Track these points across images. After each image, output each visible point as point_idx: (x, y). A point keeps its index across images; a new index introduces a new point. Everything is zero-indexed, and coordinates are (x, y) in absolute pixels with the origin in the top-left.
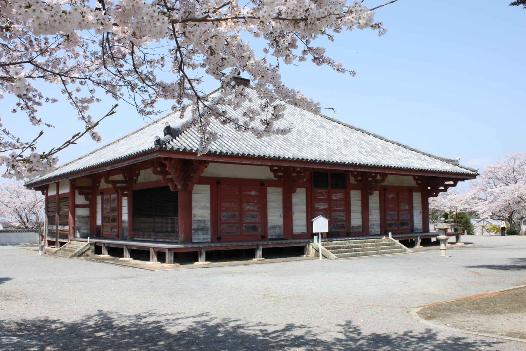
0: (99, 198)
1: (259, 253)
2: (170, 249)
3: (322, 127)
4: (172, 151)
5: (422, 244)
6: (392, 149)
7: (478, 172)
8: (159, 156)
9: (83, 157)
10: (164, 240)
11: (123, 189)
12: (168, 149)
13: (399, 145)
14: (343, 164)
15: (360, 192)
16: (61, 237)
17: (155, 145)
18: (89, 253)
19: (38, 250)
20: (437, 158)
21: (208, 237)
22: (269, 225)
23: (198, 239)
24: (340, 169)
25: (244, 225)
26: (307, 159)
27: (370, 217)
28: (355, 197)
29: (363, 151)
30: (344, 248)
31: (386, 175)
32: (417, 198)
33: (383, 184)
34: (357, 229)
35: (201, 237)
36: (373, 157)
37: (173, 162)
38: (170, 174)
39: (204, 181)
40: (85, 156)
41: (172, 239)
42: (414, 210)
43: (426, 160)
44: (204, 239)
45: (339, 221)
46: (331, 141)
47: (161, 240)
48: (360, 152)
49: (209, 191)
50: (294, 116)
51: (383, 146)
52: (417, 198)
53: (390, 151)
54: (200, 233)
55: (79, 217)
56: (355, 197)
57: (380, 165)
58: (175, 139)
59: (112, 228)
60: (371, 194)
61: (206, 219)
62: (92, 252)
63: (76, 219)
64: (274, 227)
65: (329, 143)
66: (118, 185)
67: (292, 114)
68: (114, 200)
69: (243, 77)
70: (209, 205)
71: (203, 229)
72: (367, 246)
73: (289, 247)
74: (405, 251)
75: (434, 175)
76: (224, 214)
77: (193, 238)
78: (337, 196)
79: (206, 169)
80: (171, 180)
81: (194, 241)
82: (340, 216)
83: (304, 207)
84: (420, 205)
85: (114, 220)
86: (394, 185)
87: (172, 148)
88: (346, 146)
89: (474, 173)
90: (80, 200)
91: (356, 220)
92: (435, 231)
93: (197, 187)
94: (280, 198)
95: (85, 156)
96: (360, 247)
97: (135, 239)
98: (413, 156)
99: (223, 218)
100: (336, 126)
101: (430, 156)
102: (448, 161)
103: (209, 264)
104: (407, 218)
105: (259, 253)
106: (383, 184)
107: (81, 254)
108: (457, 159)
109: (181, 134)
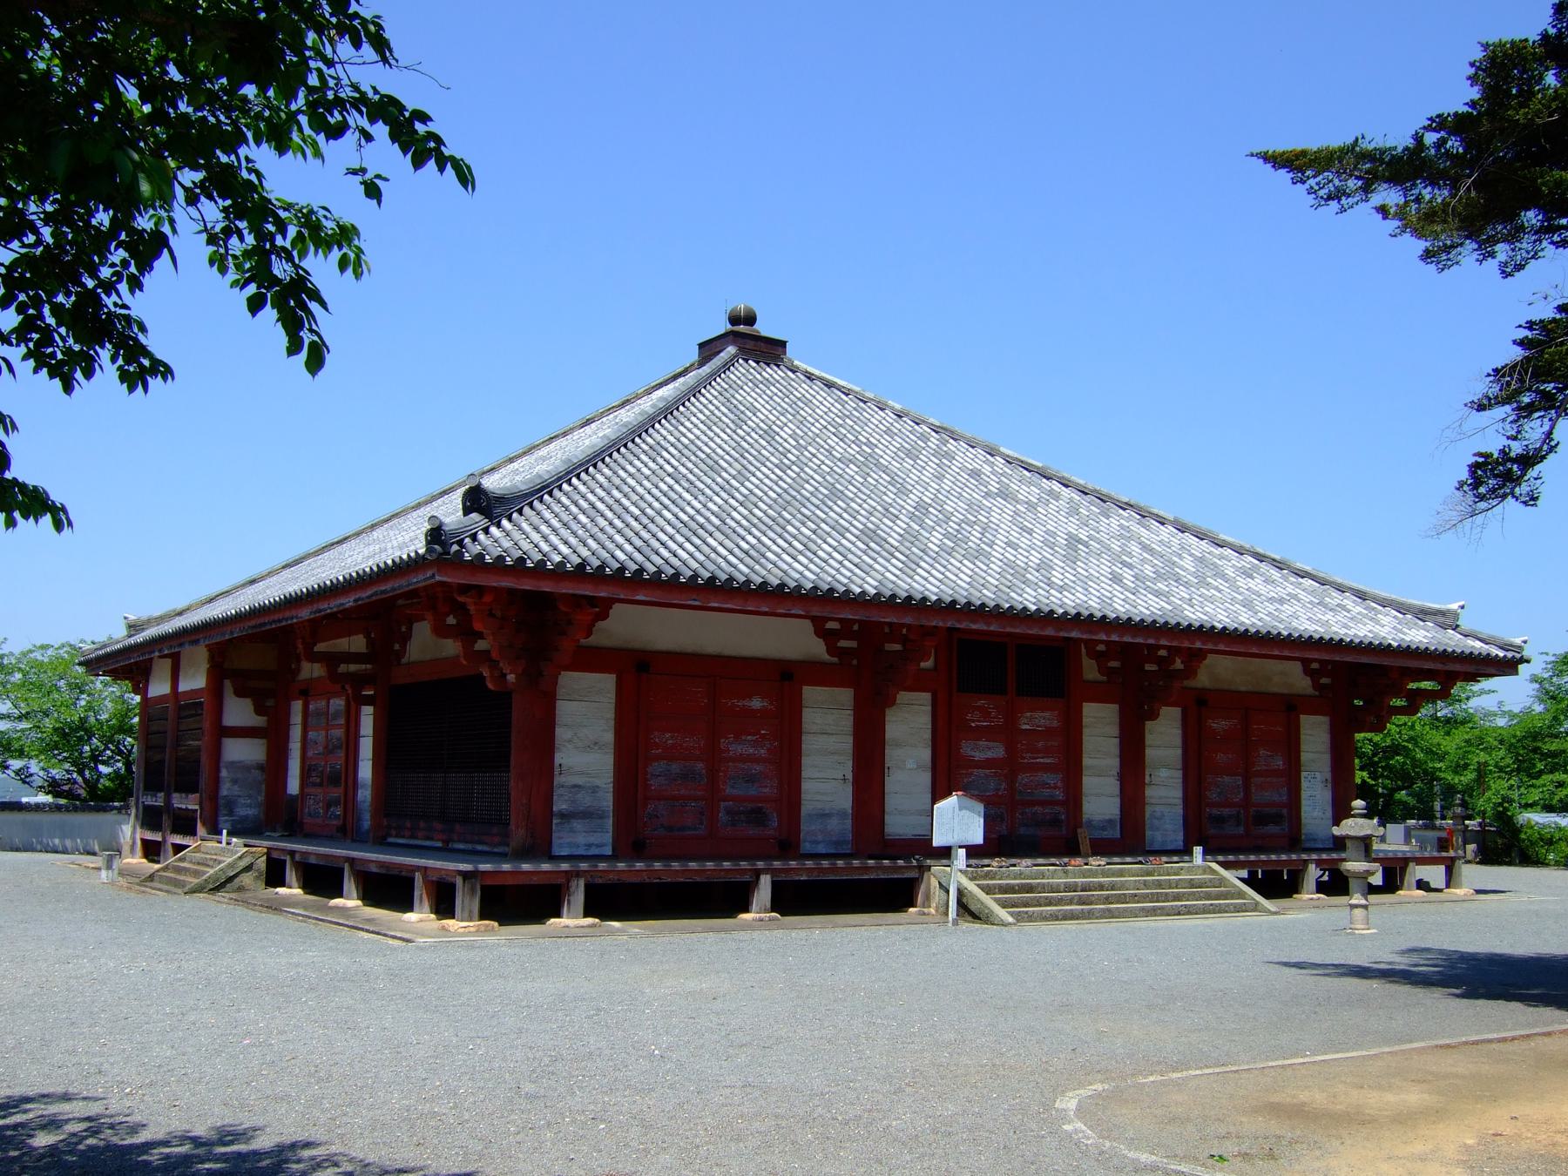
0: (297, 707)
1: (763, 892)
2: (466, 875)
3: (1005, 494)
4: (479, 562)
5: (1321, 888)
6: (1230, 572)
7: (1526, 653)
8: (438, 578)
9: (262, 578)
10: (470, 847)
11: (359, 681)
12: (467, 557)
13: (1261, 558)
14: (1046, 618)
15: (1115, 707)
16: (177, 830)
17: (428, 543)
18: (247, 879)
19: (99, 869)
20: (1385, 603)
21: (603, 839)
22: (806, 808)
23: (570, 845)
24: (1034, 631)
25: (723, 804)
26: (925, 599)
27: (1149, 792)
28: (1100, 727)
29: (1128, 575)
30: (1043, 888)
31: (1200, 655)
32: (1314, 736)
33: (1187, 683)
34: (1104, 828)
35: (581, 839)
36: (1158, 594)
37: (487, 598)
38: (481, 636)
39: (594, 660)
40: (270, 574)
41: (495, 846)
42: (1303, 774)
43: (1344, 608)
44: (590, 846)
45: (1043, 803)
46: (1024, 542)
47: (461, 846)
48: (1116, 579)
49: (612, 695)
50: (915, 458)
51: (1201, 560)
52: (1314, 736)
53: (1224, 577)
54: (577, 825)
55: (233, 765)
56: (1100, 727)
57: (1173, 622)
58: (499, 525)
59: (328, 805)
60: (1154, 716)
61: (598, 782)
62: (257, 878)
63: (224, 773)
64: (824, 816)
65: (1015, 547)
66: (343, 668)
67: (908, 454)
68: (337, 715)
69: (764, 333)
70: (609, 737)
71: (587, 815)
72: (1123, 886)
73: (874, 878)
74: (1255, 907)
75: (1364, 660)
76: (657, 767)
77: (556, 841)
78: (1038, 719)
79: (601, 624)
80: (485, 654)
81: (557, 851)
82: (1045, 785)
83: (926, 754)
84: (1326, 759)
85: (334, 779)
86: (1233, 688)
87: (480, 556)
88: (1071, 559)
89: (1510, 655)
90: (238, 712)
91: (1100, 800)
92: (1405, 848)
93: (570, 681)
94: (846, 720)
95: (270, 574)
96: (1101, 887)
97: (391, 840)
98: (1302, 595)
99: (654, 783)
100: (1051, 493)
101: (1362, 596)
102: (1423, 614)
103: (593, 926)
104: (1276, 798)
105: (763, 892)
106: (1187, 683)
107: (220, 886)
108: (1454, 606)
109: (520, 512)
